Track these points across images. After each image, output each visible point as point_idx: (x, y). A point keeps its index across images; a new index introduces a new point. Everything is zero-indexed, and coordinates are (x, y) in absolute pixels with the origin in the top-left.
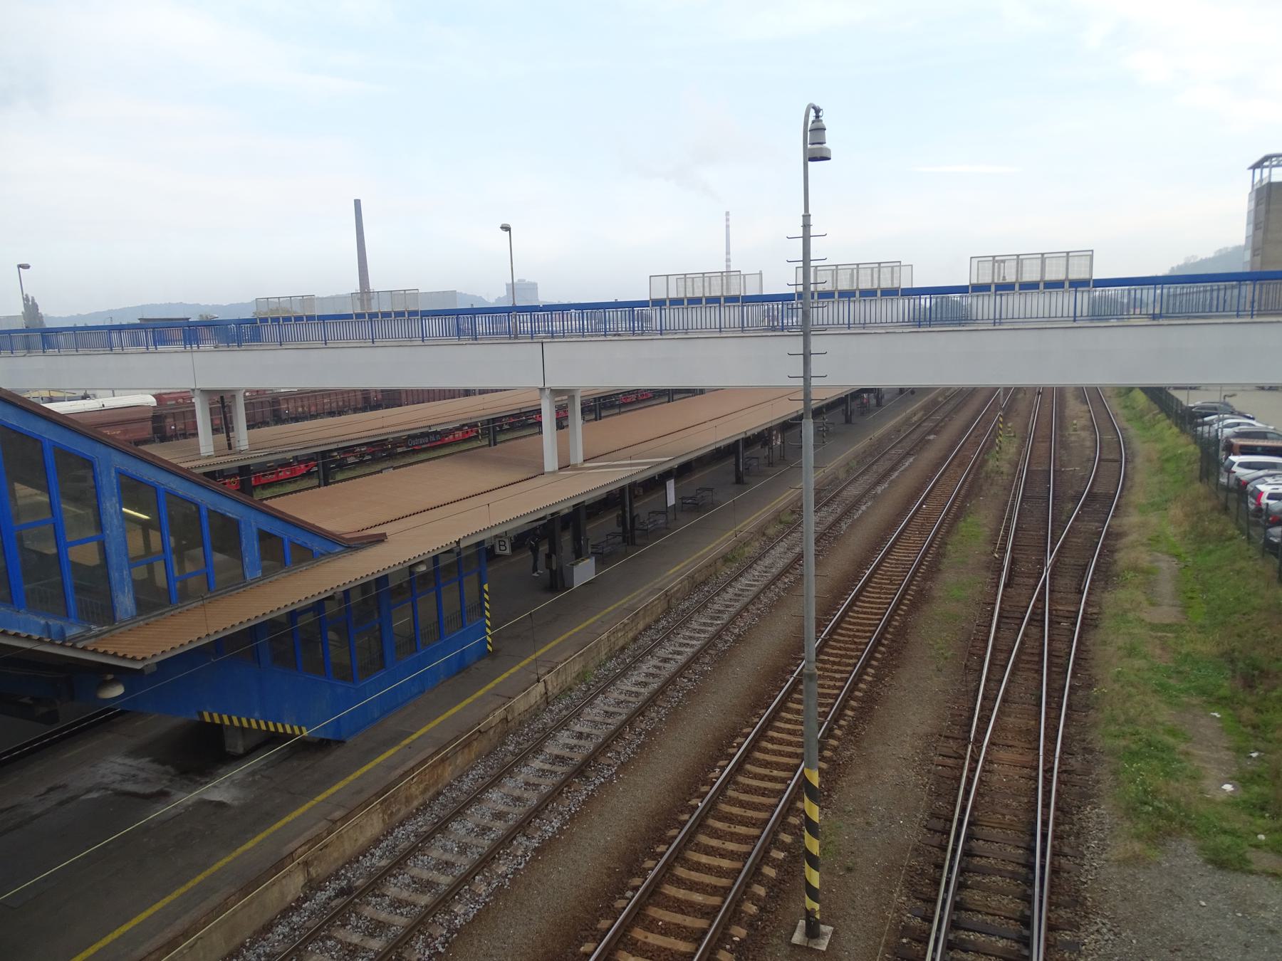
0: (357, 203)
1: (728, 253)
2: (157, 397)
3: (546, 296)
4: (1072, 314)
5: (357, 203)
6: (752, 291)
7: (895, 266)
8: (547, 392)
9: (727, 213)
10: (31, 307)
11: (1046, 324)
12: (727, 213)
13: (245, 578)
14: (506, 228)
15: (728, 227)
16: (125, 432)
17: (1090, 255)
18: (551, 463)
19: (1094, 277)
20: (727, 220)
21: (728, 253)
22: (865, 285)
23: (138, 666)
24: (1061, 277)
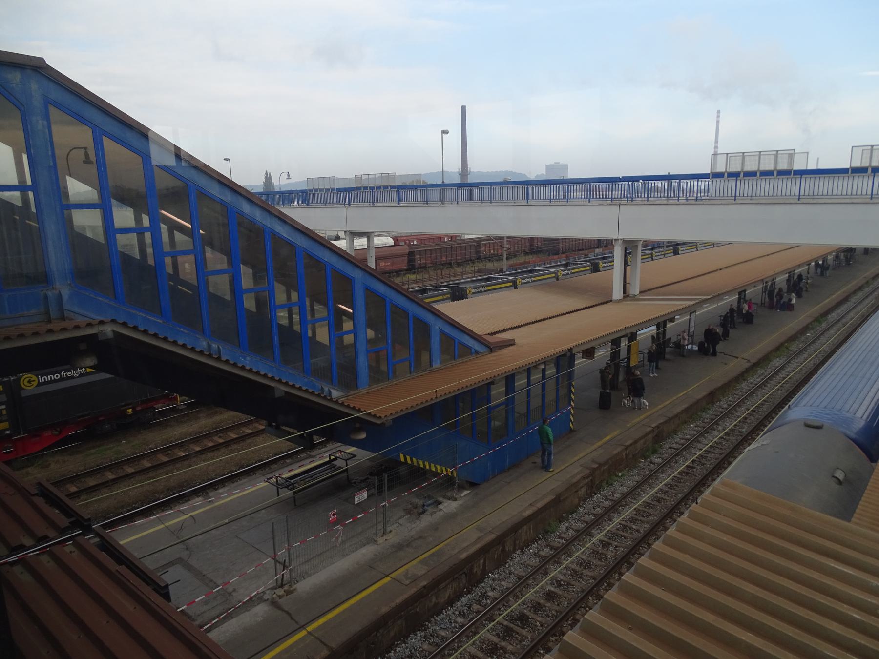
0: (464, 108)
1: (716, 142)
2: (396, 239)
3: (572, 175)
4: (797, 194)
5: (464, 108)
6: (812, 166)
7: (791, 155)
8: (620, 242)
9: (719, 112)
10: (268, 178)
11: (852, 200)
12: (719, 112)
13: (431, 365)
14: (227, 160)
15: (718, 122)
16: (392, 264)
17: (791, 155)
18: (617, 294)
19: (795, 168)
20: (718, 117)
21: (716, 142)
22: (749, 168)
23: (379, 422)
24: (866, 164)
